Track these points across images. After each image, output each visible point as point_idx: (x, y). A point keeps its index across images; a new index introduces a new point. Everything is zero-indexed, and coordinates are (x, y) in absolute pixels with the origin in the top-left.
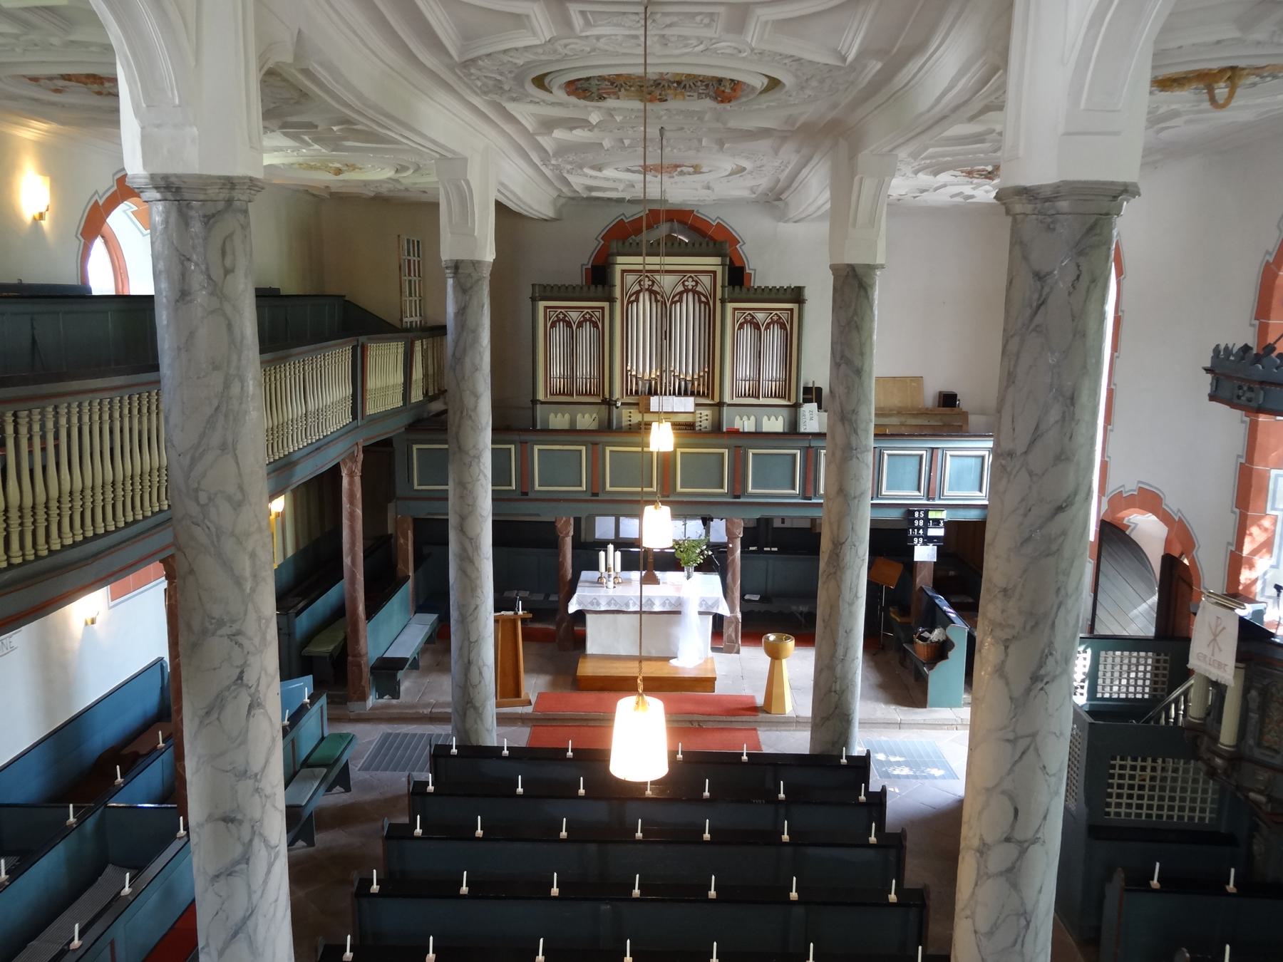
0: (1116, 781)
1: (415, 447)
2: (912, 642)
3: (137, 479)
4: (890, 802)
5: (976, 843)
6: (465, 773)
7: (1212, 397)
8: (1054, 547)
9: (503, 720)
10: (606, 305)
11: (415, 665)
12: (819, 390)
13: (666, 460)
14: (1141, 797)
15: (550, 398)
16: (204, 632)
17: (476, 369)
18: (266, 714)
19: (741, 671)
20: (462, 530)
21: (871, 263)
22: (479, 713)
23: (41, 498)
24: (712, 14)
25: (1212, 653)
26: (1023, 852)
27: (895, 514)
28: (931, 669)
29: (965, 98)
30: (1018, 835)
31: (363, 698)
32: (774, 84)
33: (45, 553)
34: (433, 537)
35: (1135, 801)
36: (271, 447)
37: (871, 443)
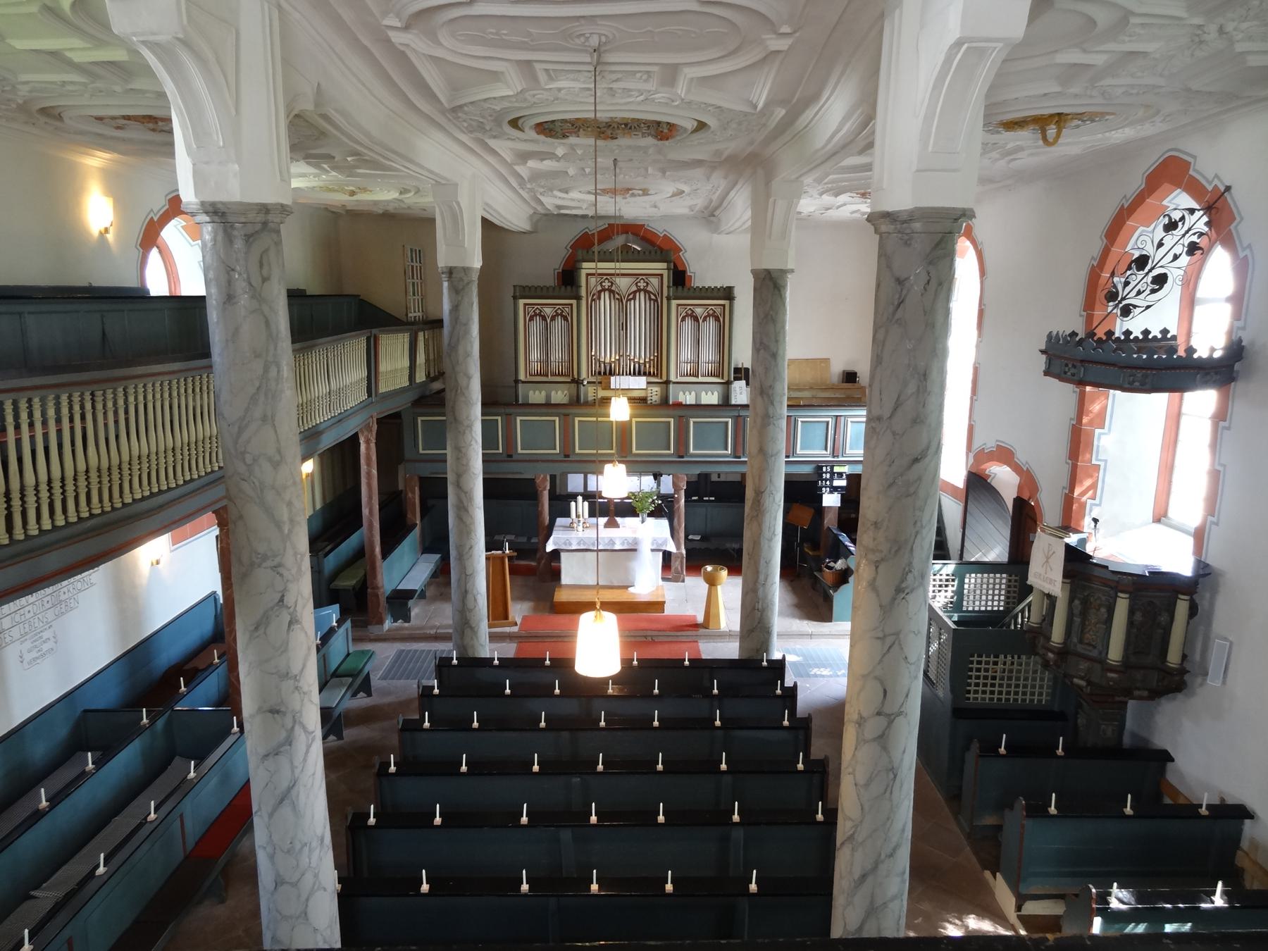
0: (974, 673)
1: (420, 419)
2: (820, 570)
3: (193, 446)
4: (801, 697)
5: (855, 717)
6: (464, 678)
7: (1047, 373)
8: (912, 490)
9: (494, 638)
10: (574, 302)
11: (422, 595)
12: (747, 370)
13: (624, 428)
14: (993, 685)
16: (252, 565)
17: (468, 355)
18: (303, 629)
19: (685, 598)
20: (458, 485)
22: (474, 631)
23: (115, 461)
24: (648, 72)
25: (1046, 572)
26: (891, 722)
27: (807, 469)
28: (835, 591)
30: (887, 710)
31: (381, 622)
32: (701, 126)
33: (119, 505)
34: (435, 492)
35: (988, 689)
36: (301, 419)
37: (785, 412)
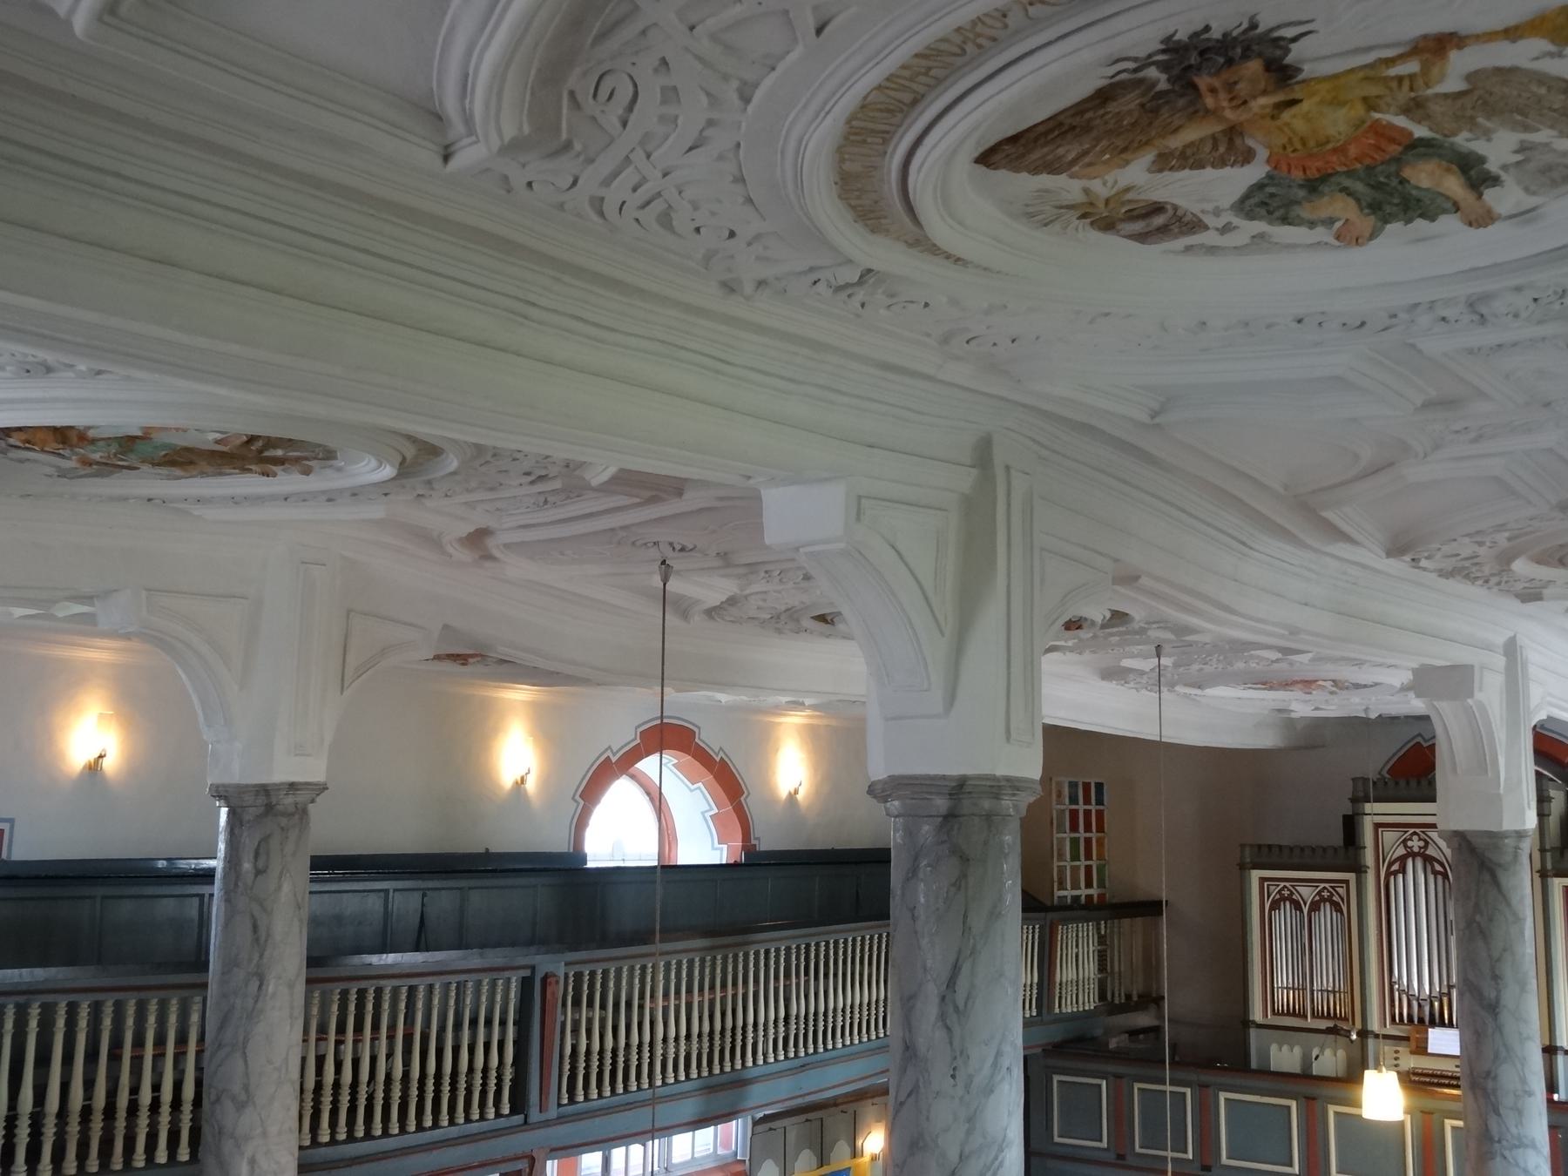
1: (1056, 1078)
10: (1351, 876)
15: (1271, 1019)
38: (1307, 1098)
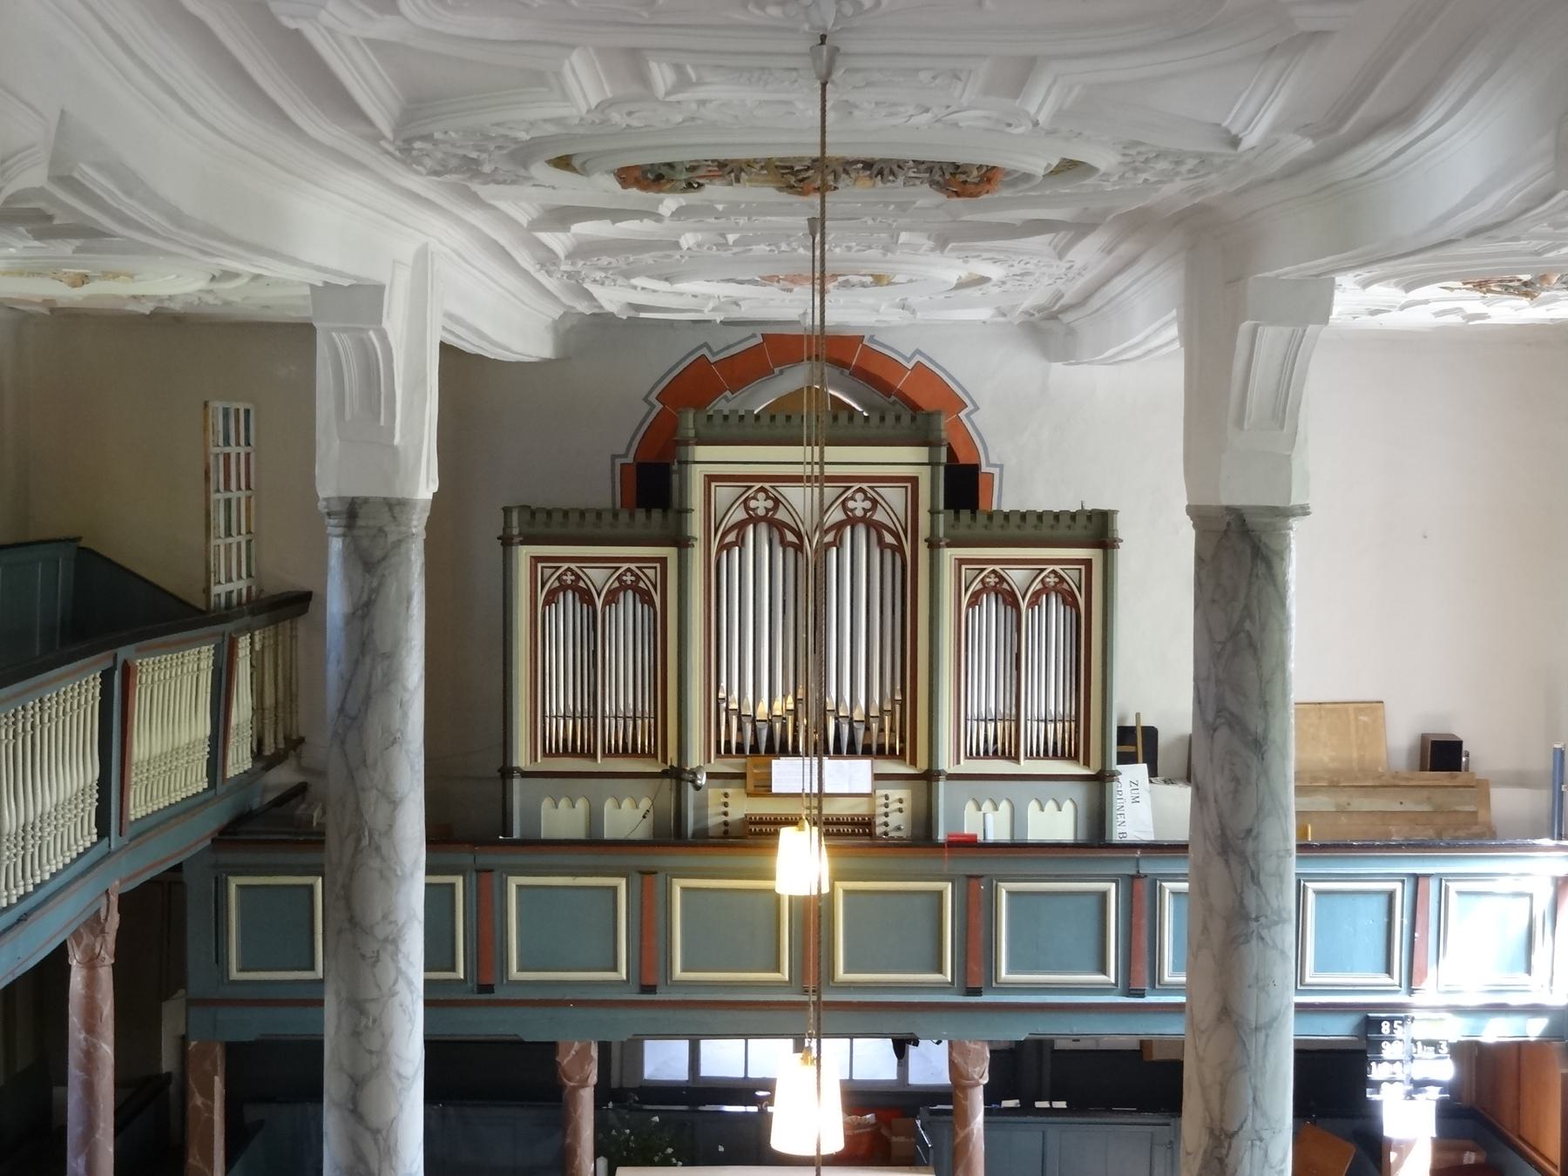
1: (234, 883)
10: (670, 553)
12: (1151, 734)
15: (543, 764)
17: (392, 740)
20: (355, 1111)
21: (1277, 502)
27: (1338, 1030)
29: (1500, 219)
38: (642, 873)
